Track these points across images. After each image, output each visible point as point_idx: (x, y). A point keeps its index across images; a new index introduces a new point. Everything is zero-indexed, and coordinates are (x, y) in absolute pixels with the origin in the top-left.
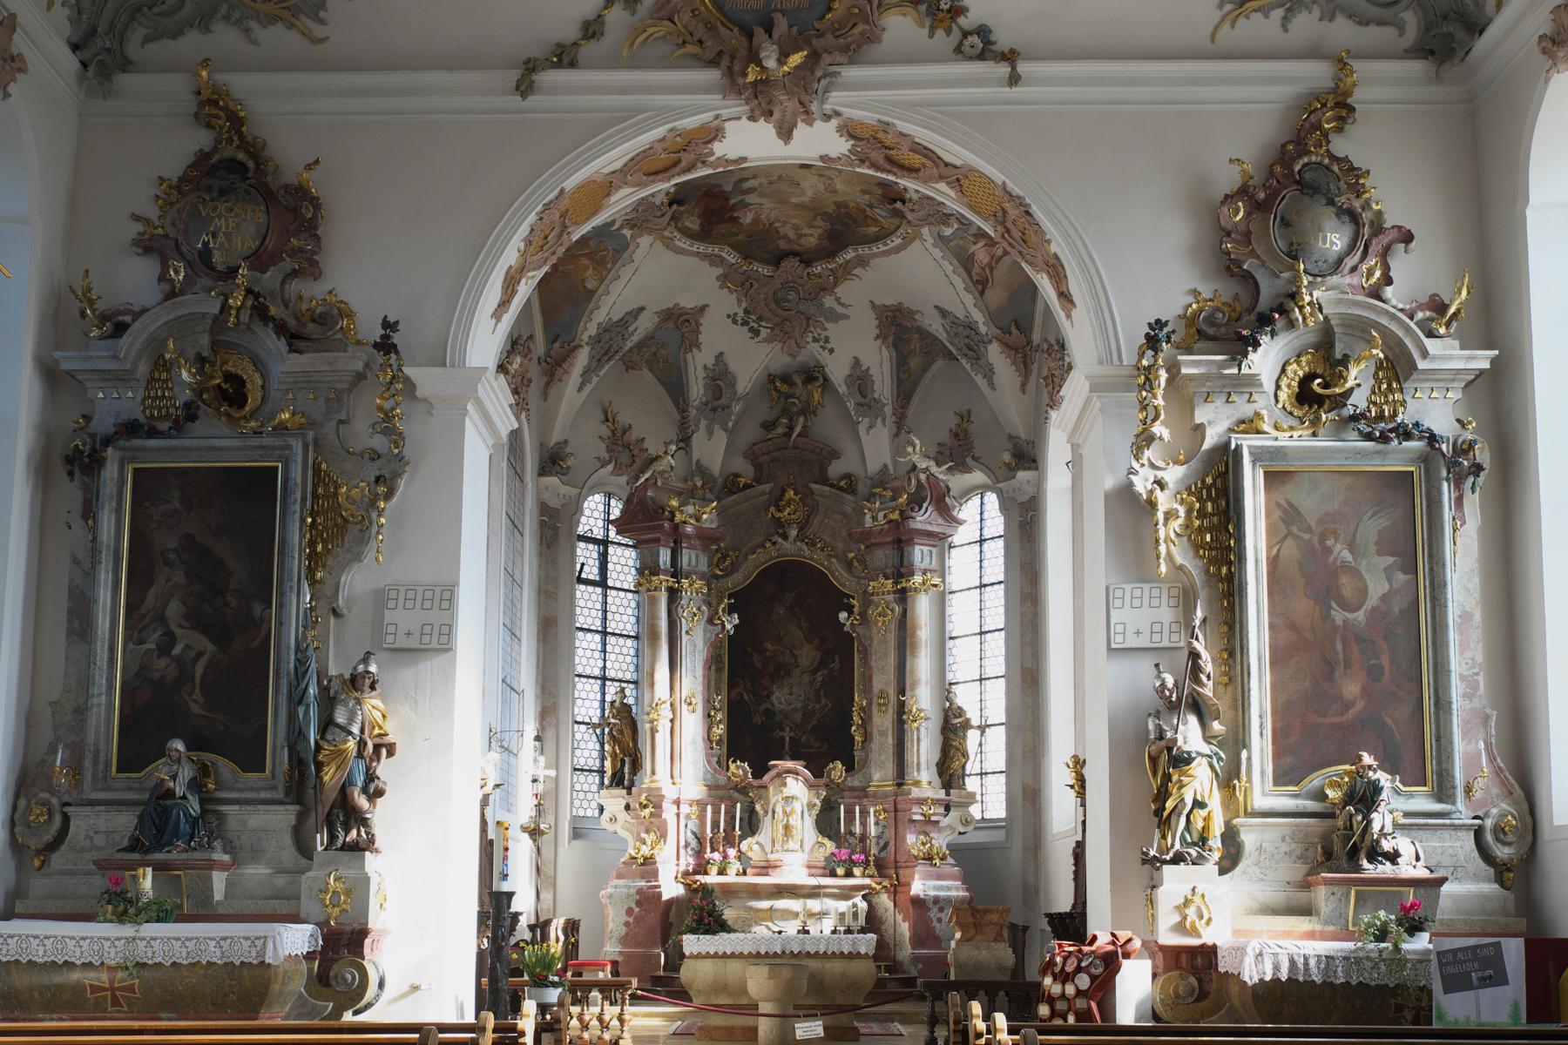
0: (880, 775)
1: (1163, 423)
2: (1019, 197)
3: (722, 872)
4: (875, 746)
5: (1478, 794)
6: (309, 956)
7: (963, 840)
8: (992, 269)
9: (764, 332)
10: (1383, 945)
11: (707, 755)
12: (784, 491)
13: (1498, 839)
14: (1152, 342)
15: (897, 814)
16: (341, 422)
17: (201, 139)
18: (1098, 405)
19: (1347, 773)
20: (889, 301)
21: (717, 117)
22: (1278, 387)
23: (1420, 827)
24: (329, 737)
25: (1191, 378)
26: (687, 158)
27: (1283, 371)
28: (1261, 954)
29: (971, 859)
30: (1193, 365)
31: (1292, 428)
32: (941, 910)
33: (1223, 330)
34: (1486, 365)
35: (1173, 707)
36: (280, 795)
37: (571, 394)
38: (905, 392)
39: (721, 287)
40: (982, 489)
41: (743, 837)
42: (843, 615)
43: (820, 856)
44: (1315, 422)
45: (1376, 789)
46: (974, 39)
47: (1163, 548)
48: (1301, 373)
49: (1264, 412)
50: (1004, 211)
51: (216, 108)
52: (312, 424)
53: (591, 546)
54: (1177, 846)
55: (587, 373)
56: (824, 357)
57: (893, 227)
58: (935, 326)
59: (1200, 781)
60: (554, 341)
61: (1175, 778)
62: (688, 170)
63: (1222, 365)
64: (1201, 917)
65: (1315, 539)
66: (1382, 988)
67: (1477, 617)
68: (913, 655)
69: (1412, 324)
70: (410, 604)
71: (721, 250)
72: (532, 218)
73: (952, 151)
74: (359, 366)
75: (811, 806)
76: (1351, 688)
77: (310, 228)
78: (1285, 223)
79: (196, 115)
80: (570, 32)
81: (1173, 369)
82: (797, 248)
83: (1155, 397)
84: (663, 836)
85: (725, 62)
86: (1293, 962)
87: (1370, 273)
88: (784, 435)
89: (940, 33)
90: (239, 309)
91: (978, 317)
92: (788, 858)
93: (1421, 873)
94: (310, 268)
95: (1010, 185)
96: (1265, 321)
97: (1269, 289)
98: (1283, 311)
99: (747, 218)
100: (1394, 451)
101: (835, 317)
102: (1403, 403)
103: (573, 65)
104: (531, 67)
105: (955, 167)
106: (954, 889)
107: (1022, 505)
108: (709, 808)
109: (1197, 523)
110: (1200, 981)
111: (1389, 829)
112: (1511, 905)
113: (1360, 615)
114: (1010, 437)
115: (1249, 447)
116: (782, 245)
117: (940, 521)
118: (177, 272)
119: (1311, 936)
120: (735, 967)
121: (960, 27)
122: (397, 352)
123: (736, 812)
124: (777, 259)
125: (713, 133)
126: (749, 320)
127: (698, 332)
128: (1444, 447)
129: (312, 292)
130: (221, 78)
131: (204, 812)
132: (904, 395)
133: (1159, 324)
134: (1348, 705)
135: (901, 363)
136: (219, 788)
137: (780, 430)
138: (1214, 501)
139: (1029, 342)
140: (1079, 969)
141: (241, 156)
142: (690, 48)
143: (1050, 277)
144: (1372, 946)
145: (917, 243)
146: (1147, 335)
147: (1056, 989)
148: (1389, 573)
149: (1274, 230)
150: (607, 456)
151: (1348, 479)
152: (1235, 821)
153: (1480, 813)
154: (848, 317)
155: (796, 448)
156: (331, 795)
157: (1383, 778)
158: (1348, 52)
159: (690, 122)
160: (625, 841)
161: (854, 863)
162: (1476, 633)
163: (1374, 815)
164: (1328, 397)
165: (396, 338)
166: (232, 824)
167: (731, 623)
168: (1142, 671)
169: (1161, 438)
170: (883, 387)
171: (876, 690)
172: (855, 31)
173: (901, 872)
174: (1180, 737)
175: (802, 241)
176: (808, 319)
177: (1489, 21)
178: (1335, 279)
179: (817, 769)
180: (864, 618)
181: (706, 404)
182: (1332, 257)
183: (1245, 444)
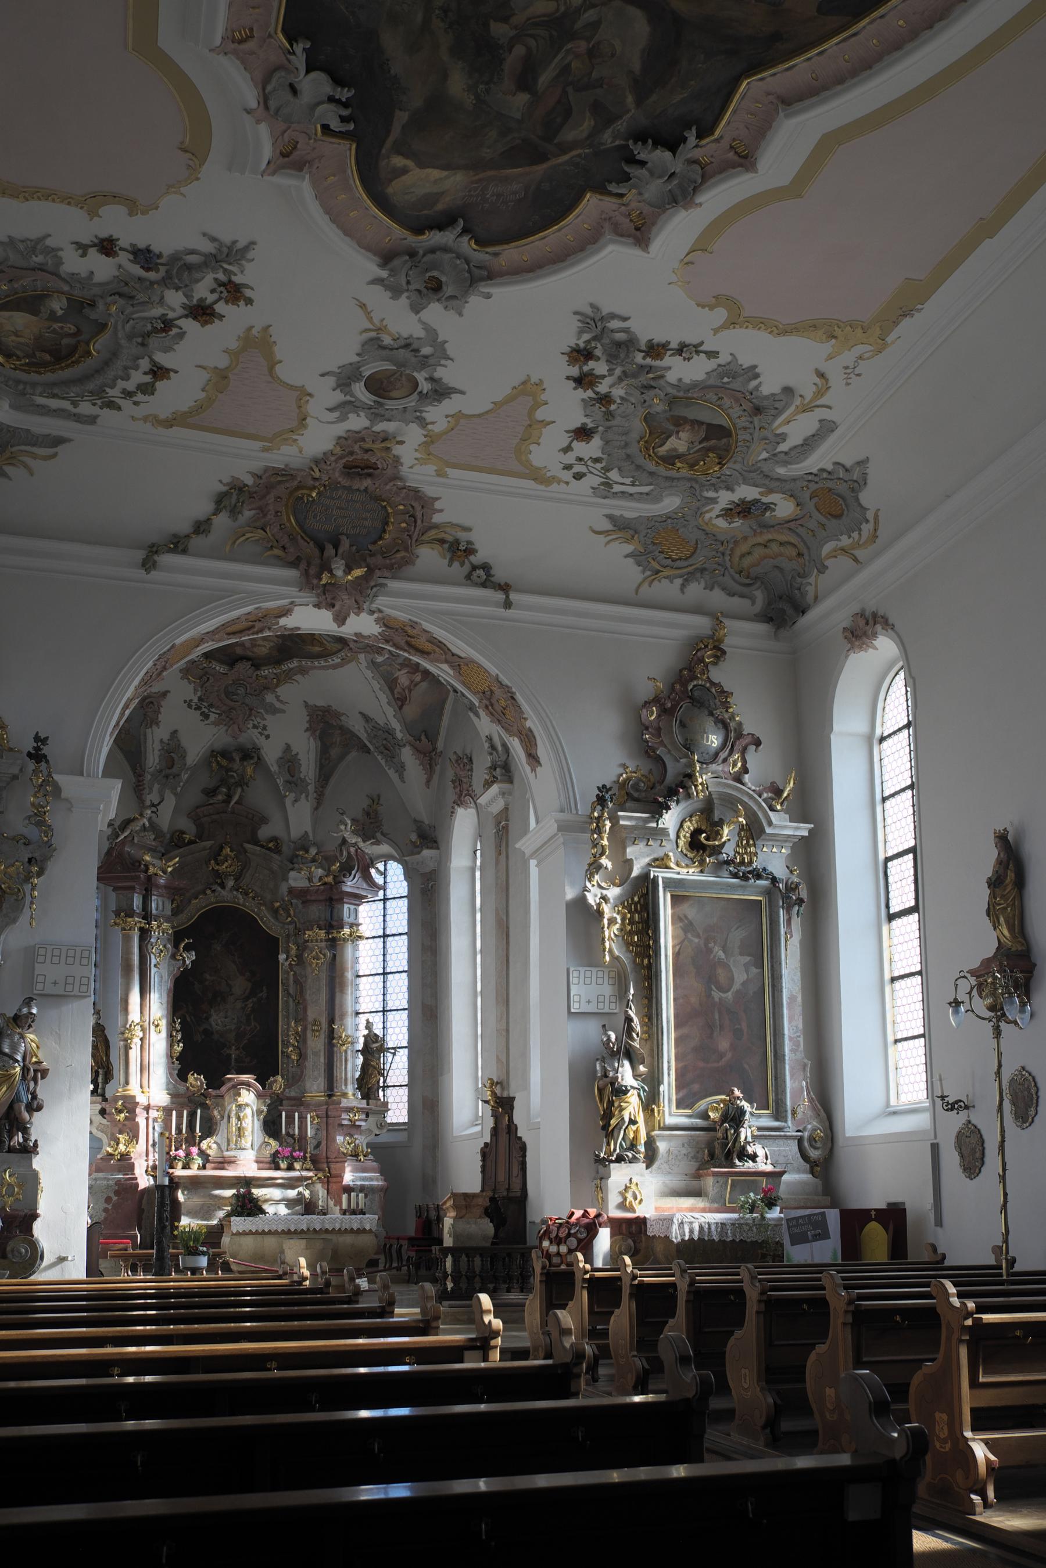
0: (315, 1089)
2: (507, 686)
4: (309, 1063)
5: (799, 1116)
7: (379, 1140)
8: (410, 691)
9: (213, 717)
12: (221, 848)
13: (811, 1145)
14: (601, 801)
15: (329, 1119)
18: (561, 840)
19: (722, 1101)
20: (320, 703)
21: (292, 603)
22: (678, 837)
26: (258, 625)
27: (681, 826)
28: (682, 1223)
29: (385, 1154)
30: (628, 818)
31: (687, 866)
33: (643, 794)
34: (806, 834)
35: (614, 1055)
38: (325, 772)
40: (386, 858)
43: (268, 1152)
44: (702, 862)
45: (742, 1112)
46: (481, 572)
47: (607, 945)
49: (671, 854)
50: (492, 692)
54: (618, 1151)
56: (261, 741)
57: (334, 649)
58: (358, 727)
59: (632, 1105)
61: (616, 1104)
62: (257, 633)
64: (635, 1198)
65: (702, 942)
66: (754, 1243)
67: (799, 999)
69: (760, 800)
70: (56, 960)
73: (459, 647)
75: (259, 1112)
76: (724, 1044)
78: (683, 725)
80: (184, 527)
81: (615, 820)
84: (134, 1136)
85: (303, 565)
86: (701, 1228)
88: (224, 801)
89: (456, 564)
91: (396, 725)
93: (769, 1168)
95: (502, 677)
96: (672, 793)
97: (673, 769)
100: (751, 886)
101: (274, 711)
102: (756, 854)
103: (184, 551)
105: (460, 657)
106: (375, 1179)
107: (423, 875)
108: (174, 1113)
109: (629, 928)
110: (634, 1242)
111: (749, 1139)
112: (820, 1188)
113: (729, 995)
114: (415, 821)
117: (365, 886)
120: (271, 1242)
122: (47, 762)
123: (197, 1112)
126: (202, 707)
132: (325, 775)
133: (603, 788)
134: (721, 1056)
135: (324, 751)
137: (220, 797)
138: (639, 913)
139: (435, 749)
140: (569, 1235)
143: (521, 741)
144: (748, 1216)
145: (353, 664)
147: (553, 1249)
148: (746, 966)
149: (676, 729)
152: (653, 1133)
153: (800, 1128)
154: (284, 711)
155: (233, 813)
157: (745, 1105)
160: (100, 1140)
161: (296, 1159)
162: (798, 1010)
163: (742, 1129)
165: (45, 750)
167: (190, 958)
168: (591, 1030)
169: (606, 868)
170: (308, 769)
171: (310, 1019)
172: (398, 555)
173: (332, 1166)
174: (619, 1075)
175: (255, 650)
178: (713, 767)
181: (160, 771)
182: (712, 752)
183: (660, 875)
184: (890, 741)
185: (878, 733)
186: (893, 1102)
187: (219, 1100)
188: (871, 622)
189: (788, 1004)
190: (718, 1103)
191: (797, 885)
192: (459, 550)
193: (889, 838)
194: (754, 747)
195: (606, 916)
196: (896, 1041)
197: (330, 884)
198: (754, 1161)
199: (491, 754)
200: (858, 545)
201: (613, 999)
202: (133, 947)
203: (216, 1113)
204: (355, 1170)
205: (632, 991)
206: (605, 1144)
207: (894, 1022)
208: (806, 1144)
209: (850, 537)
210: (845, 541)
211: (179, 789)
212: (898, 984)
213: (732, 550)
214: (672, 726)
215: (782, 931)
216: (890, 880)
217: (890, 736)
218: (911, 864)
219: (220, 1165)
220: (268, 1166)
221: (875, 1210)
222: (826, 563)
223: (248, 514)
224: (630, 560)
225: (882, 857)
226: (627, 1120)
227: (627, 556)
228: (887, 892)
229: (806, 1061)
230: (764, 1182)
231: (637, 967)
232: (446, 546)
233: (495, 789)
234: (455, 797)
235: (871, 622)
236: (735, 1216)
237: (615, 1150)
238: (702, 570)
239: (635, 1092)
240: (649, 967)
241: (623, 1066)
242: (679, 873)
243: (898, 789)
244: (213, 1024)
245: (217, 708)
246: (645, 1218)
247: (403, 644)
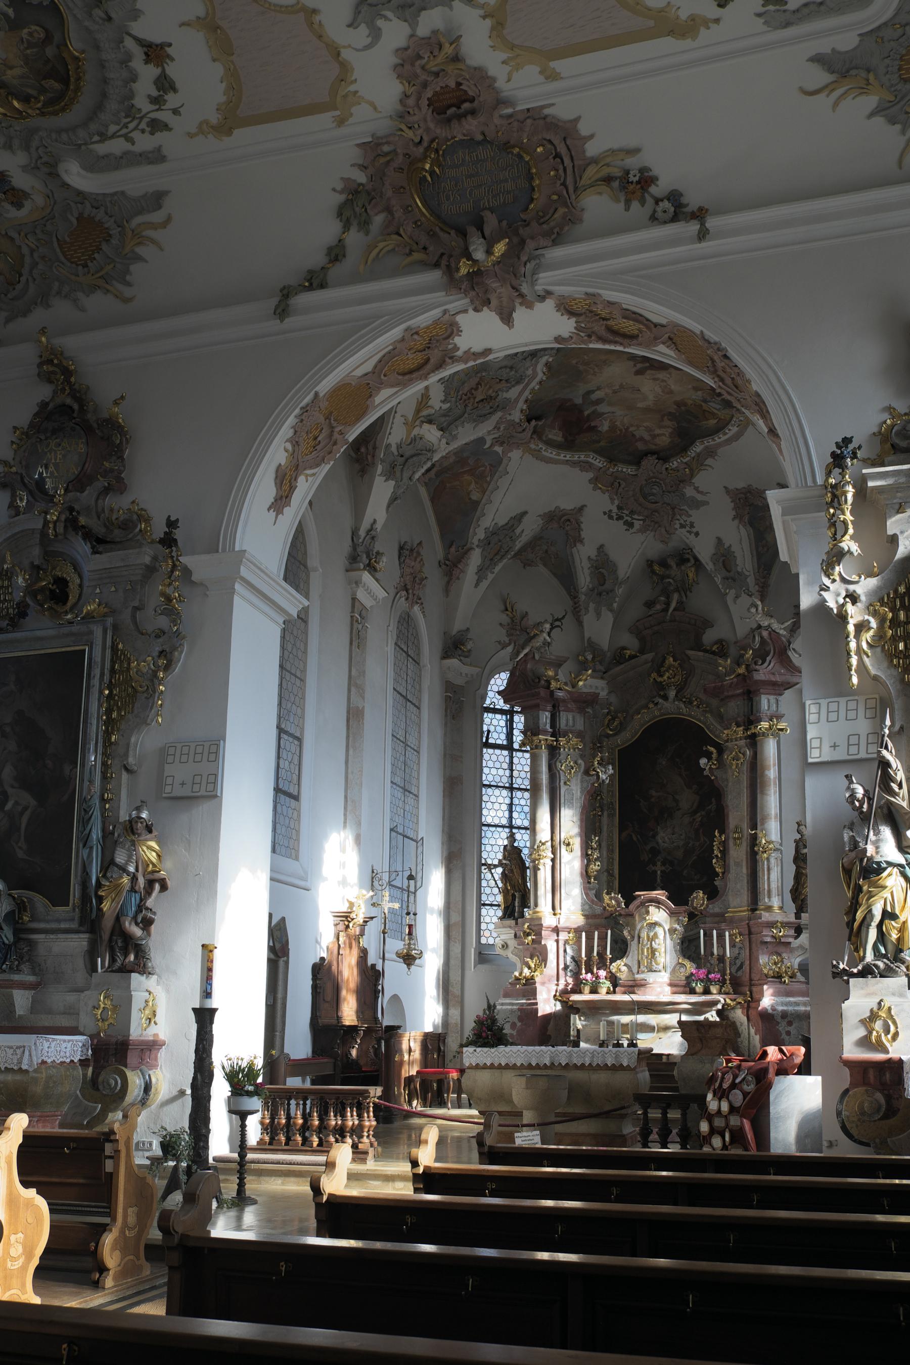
0: (736, 901)
1: (852, 538)
2: (716, 343)
3: (594, 991)
4: (731, 876)
6: (84, 1063)
9: (637, 525)
11: (585, 888)
12: (664, 659)
14: (838, 460)
16: (136, 609)
17: (44, 392)
21: (445, 312)
24: (109, 875)
26: (435, 355)
30: (879, 478)
32: (790, 1023)
35: (865, 818)
36: (74, 925)
37: (470, 589)
39: (594, 489)
41: (613, 960)
42: (703, 761)
43: (682, 974)
46: (666, 204)
47: (854, 660)
51: (56, 368)
52: (113, 612)
53: (498, 716)
55: (481, 572)
56: (691, 540)
60: (450, 546)
61: (865, 888)
64: (887, 1031)
68: (763, 793)
71: (588, 456)
72: (291, 420)
73: (658, 312)
74: (147, 560)
75: (672, 931)
77: (117, 452)
79: (39, 375)
80: (317, 259)
82: (654, 447)
83: (844, 514)
84: (544, 960)
85: (444, 262)
89: (635, 205)
90: (55, 523)
92: (650, 977)
94: (117, 485)
95: (708, 334)
99: (605, 427)
101: (696, 504)
103: (322, 286)
104: (286, 293)
105: (663, 326)
110: (888, 1098)
116: (641, 446)
118: (21, 500)
120: (509, 1076)
121: (652, 196)
123: (610, 935)
124: (637, 459)
125: (453, 329)
126: (623, 515)
127: (579, 529)
129: (119, 504)
130: (57, 342)
131: (17, 940)
136: (33, 919)
137: (658, 607)
140: (733, 1086)
141: (69, 401)
142: (417, 256)
150: (507, 640)
154: (706, 503)
156: (108, 923)
159: (423, 320)
166: (41, 950)
169: (849, 552)
176: (673, 509)
179: (679, 897)
180: (721, 764)
181: (592, 590)
187: (629, 919)
192: (635, 185)
197: (743, 675)
202: (541, 765)
203: (626, 933)
204: (776, 994)
211: (615, 605)
219: (631, 989)
220: (681, 989)
223: (378, 220)
224: (879, 120)
227: (872, 115)
232: (616, 184)
244: (660, 841)
245: (639, 514)
247: (603, 332)
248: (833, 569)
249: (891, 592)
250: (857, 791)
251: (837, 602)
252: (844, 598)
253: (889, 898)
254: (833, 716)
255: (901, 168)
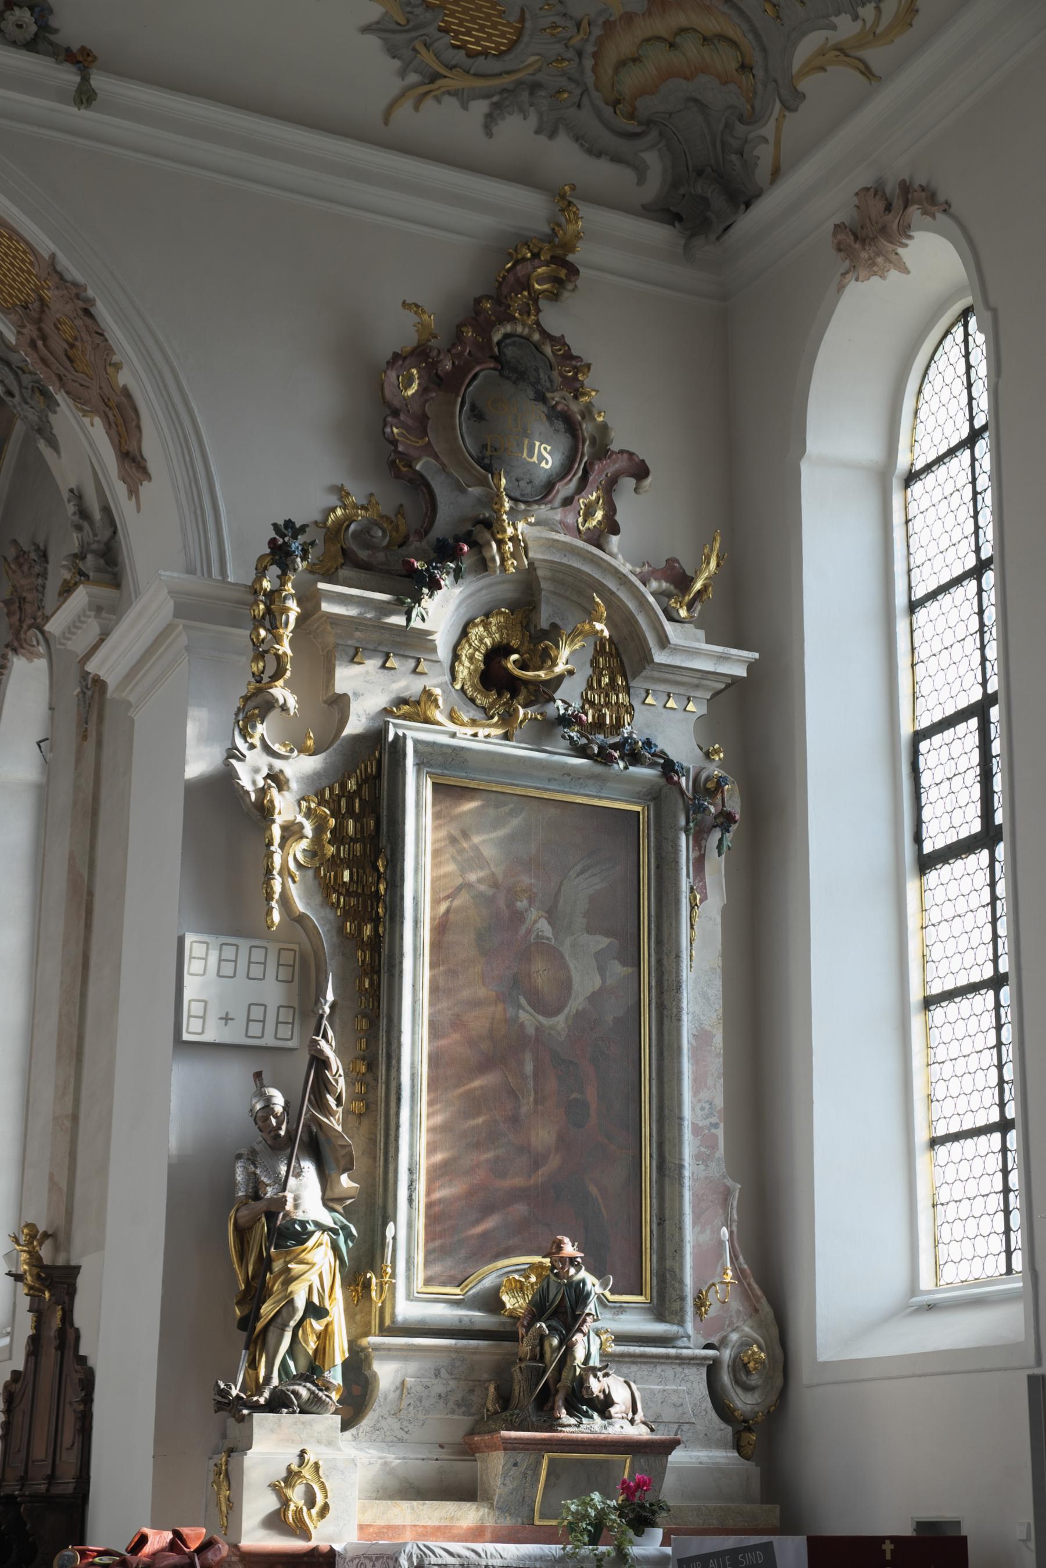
1: (287, 685)
2: (75, 284)
5: (713, 1310)
10: (602, 1549)
13: (737, 1381)
14: (279, 555)
18: (183, 640)
19: (533, 1267)
22: (456, 657)
23: (634, 1359)
25: (335, 620)
27: (464, 634)
30: (342, 600)
31: (474, 722)
33: (381, 556)
34: (741, 672)
35: (280, 1146)
44: (508, 718)
45: (580, 1295)
47: (277, 885)
48: (488, 641)
49: (437, 691)
50: (43, 302)
54: (275, 1382)
59: (317, 1268)
61: (277, 1266)
63: (385, 609)
64: (311, 1502)
67: (718, 1040)
78: (477, 414)
81: (309, 600)
83: (278, 640)
87: (589, 514)
93: (639, 1432)
95: (64, 262)
96: (445, 552)
97: (450, 509)
98: (477, 546)
100: (618, 778)
102: (630, 709)
109: (331, 850)
111: (595, 1361)
113: (560, 1021)
115: (416, 742)
119: (477, 1534)
128: (683, 780)
138: (357, 819)
143: (109, 425)
144: (586, 1550)
146: (272, 542)
149: (461, 421)
151: (552, 811)
153: (714, 1340)
158: (573, 187)
162: (716, 1064)
163: (578, 1337)
164: (526, 682)
168: (232, 1080)
169: (284, 708)
174: (290, 1196)
177: (759, 194)
182: (540, 479)
184: (929, 479)
185: (903, 462)
186: (926, 1282)
188: (897, 203)
189: (695, 1051)
190: (525, 1273)
191: (720, 784)
193: (925, 688)
194: (631, 482)
195: (279, 820)
196: (934, 1142)
198: (605, 1415)
199: (79, 528)
200: (871, 37)
201: (286, 1015)
205: (330, 996)
206: (243, 1365)
207: (930, 1099)
208: (726, 1378)
209: (856, 17)
210: (846, 28)
212: (938, 1013)
213: (600, 42)
214: (447, 423)
215: (684, 885)
216: (925, 780)
217: (928, 468)
218: (974, 739)
221: (894, 1539)
222: (803, 86)
224: (373, 42)
225: (906, 730)
226: (300, 1304)
227: (367, 29)
228: (918, 808)
229: (729, 1182)
230: (626, 1468)
231: (348, 941)
233: (81, 596)
234: (9, 638)
235: (897, 203)
236: (554, 1549)
237: (268, 1378)
238: (534, 87)
239: (326, 1238)
240: (375, 944)
241: (298, 1175)
242: (453, 735)
243: (945, 579)
246: (332, 1552)
248: (254, 727)
249: (337, 786)
250: (275, 1100)
251: (254, 783)
252: (265, 779)
253: (316, 1284)
254: (228, 969)
255: (386, 122)
